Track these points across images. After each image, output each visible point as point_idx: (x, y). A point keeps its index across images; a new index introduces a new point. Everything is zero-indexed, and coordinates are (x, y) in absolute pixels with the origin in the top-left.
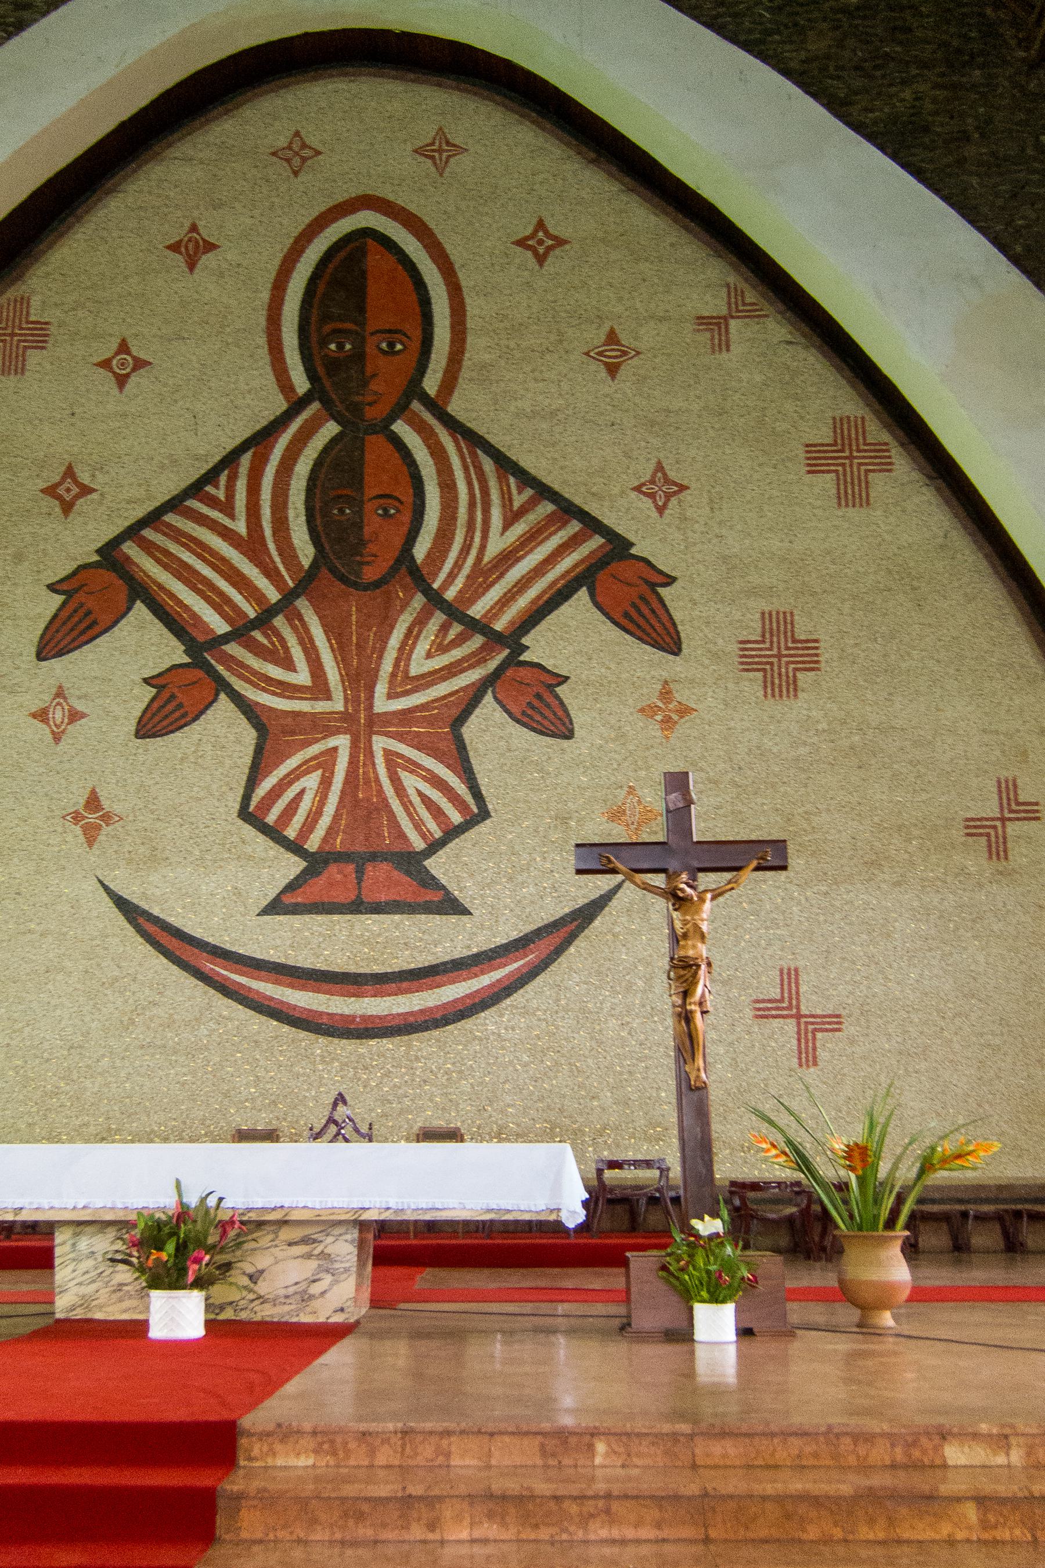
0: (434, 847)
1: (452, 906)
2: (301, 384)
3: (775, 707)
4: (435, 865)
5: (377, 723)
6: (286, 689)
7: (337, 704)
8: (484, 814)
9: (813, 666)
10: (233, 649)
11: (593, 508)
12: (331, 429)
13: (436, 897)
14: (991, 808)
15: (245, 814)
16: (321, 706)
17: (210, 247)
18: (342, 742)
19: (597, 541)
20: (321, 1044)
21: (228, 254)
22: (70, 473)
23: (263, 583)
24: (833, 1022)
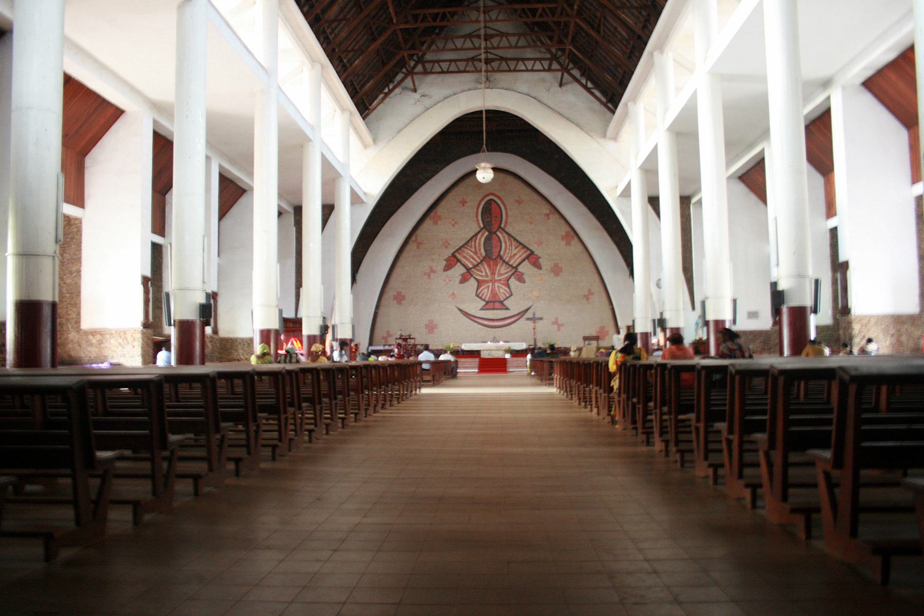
0: (505, 300)
1: (507, 309)
2: (482, 226)
4: (505, 303)
5: (496, 281)
7: (489, 278)
8: (511, 295)
10: (473, 270)
11: (528, 246)
12: (487, 233)
13: (505, 308)
14: (587, 293)
16: (487, 279)
17: (466, 202)
18: (490, 284)
20: (489, 329)
24: (563, 325)
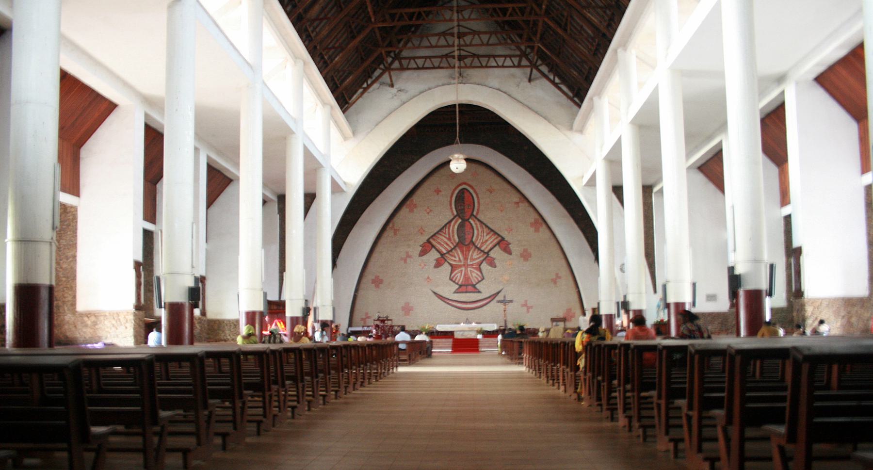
0: (477, 283)
1: (479, 292)
2: (455, 213)
3: (525, 263)
4: (477, 286)
5: (468, 265)
6: (455, 261)
8: (483, 279)
9: (530, 256)
10: (447, 255)
11: (499, 233)
12: (460, 221)
14: (554, 277)
15: (451, 279)
16: (460, 264)
17: (440, 191)
18: (463, 269)
19: (500, 238)
20: (462, 311)
21: (443, 193)
22: (422, 228)
23: (451, 245)
24: (531, 307)
